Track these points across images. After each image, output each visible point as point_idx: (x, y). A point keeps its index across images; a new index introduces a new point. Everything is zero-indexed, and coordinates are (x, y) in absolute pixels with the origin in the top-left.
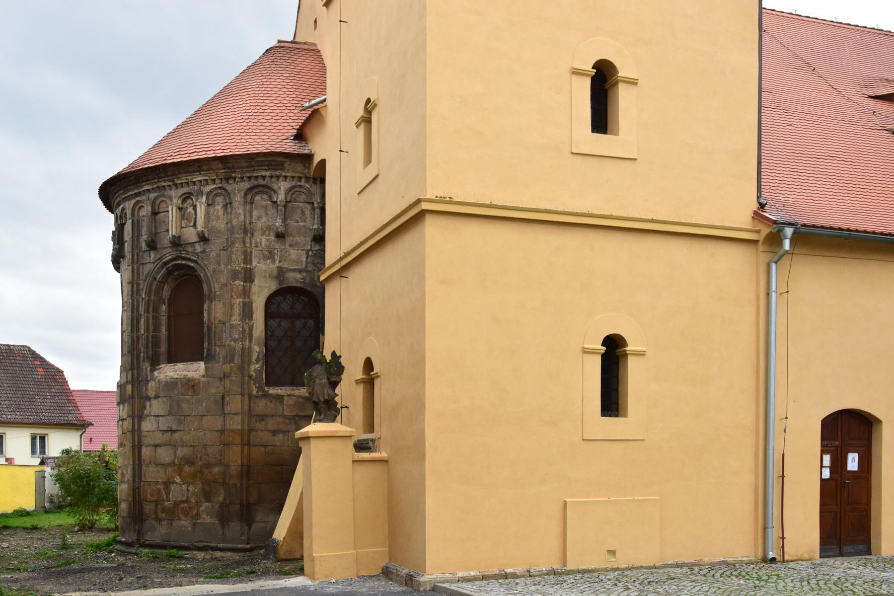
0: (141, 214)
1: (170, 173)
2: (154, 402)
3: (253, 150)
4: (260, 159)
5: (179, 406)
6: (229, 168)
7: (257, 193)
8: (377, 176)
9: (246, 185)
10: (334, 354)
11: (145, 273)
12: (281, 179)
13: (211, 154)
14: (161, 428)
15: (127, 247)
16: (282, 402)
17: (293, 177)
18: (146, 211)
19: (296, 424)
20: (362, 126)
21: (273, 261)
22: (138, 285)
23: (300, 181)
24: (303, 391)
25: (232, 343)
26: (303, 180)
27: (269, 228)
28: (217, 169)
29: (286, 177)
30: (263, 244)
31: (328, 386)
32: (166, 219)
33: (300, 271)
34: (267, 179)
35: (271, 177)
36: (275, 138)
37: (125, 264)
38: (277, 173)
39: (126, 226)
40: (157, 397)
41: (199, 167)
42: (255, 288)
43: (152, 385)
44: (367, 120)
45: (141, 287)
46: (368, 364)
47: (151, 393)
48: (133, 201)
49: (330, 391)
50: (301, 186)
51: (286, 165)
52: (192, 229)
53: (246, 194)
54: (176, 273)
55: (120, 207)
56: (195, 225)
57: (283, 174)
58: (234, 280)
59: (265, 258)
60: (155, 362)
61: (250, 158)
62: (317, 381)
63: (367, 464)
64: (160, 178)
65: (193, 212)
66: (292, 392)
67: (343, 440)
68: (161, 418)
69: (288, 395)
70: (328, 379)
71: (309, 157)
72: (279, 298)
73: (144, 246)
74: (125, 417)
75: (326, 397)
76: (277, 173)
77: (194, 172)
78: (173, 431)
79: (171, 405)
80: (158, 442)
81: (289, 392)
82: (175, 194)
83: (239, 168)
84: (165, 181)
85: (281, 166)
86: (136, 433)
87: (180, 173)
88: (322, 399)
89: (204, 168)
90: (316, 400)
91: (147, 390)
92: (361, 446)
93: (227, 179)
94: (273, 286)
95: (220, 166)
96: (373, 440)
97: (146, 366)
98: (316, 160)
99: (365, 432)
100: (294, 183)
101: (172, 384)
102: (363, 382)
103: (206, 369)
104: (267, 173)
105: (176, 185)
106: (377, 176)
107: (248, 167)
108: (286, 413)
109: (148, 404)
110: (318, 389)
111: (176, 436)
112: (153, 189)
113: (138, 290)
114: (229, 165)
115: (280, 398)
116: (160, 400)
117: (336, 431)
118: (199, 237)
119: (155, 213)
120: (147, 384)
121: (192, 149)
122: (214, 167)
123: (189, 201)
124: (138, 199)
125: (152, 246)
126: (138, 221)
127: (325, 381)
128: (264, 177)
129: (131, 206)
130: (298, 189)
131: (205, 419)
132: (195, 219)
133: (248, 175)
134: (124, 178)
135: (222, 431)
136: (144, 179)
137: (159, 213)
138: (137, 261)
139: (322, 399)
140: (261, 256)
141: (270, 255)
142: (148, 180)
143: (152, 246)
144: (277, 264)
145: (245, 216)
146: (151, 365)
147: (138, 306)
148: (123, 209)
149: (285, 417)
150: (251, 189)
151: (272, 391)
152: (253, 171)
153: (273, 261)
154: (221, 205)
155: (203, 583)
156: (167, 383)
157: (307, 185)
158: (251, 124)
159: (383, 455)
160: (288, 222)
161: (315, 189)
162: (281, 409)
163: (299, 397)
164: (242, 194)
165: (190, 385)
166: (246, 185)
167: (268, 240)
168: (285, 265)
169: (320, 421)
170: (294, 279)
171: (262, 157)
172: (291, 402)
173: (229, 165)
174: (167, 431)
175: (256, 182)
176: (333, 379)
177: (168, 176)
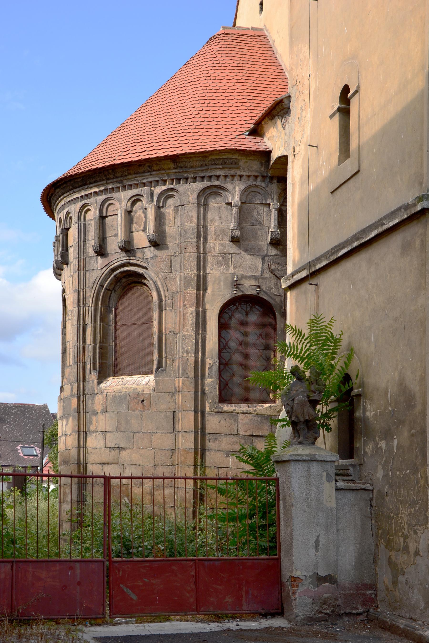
0: (87, 218)
1: (119, 175)
2: (101, 417)
3: (206, 148)
4: (214, 157)
5: (127, 421)
6: (181, 167)
7: (211, 194)
8: (358, 172)
9: (199, 186)
11: (92, 280)
12: (236, 178)
13: (162, 154)
14: (108, 445)
15: (72, 254)
17: (249, 176)
18: (92, 215)
20: (337, 118)
21: (228, 267)
22: (85, 293)
23: (256, 180)
25: (185, 355)
26: (259, 179)
27: (223, 232)
28: (169, 169)
29: (241, 176)
30: (217, 248)
32: (115, 224)
33: (256, 278)
34: (222, 178)
35: (226, 176)
36: (228, 133)
37: (69, 271)
38: (232, 172)
39: (70, 231)
40: (104, 411)
41: (149, 167)
42: (208, 296)
43: (99, 399)
44: (344, 111)
45: (88, 295)
47: (98, 407)
48: (80, 204)
49: (311, 411)
50: (256, 186)
51: (241, 163)
52: (142, 233)
53: (199, 196)
54: (124, 280)
55: (65, 211)
56: (145, 230)
57: (239, 173)
58: (186, 287)
59: (219, 264)
60: (102, 376)
61: (204, 155)
64: (109, 179)
65: (143, 215)
68: (108, 435)
69: (243, 413)
71: (268, 154)
72: (233, 308)
73: (91, 252)
74: (69, 432)
76: (232, 172)
77: (144, 172)
78: (120, 449)
79: (118, 420)
80: (105, 460)
82: (123, 197)
83: (192, 167)
84: (113, 183)
85: (235, 164)
86: (82, 449)
87: (129, 174)
88: (302, 419)
89: (155, 168)
90: (296, 420)
91: (93, 404)
93: (179, 180)
94: (227, 295)
95: (172, 165)
97: (93, 377)
98: (274, 156)
99: (342, 458)
100: (249, 183)
101: (122, 398)
103: (157, 382)
104: (221, 173)
105: (125, 186)
106: (358, 172)
107: (202, 166)
109: (94, 418)
111: (124, 454)
112: (100, 191)
113: (85, 298)
114: (181, 164)
115: (235, 414)
116: (107, 415)
118: (150, 242)
119: (102, 218)
120: (94, 397)
121: (174, 144)
122: (165, 167)
123: (139, 204)
124: (84, 202)
125: (101, 252)
126: (85, 225)
128: (218, 177)
129: (78, 210)
130: (253, 189)
131: (155, 436)
132: (145, 223)
133: (202, 175)
134: (70, 181)
135: (173, 451)
136: (92, 180)
137: (107, 216)
138: (83, 267)
139: (302, 419)
140: (215, 262)
141: (225, 259)
142: (96, 182)
143: (101, 252)
144: (231, 271)
145: (198, 219)
146: (99, 377)
147: (84, 315)
148: (68, 213)
150: (204, 189)
151: (227, 407)
152: (207, 170)
153: (228, 267)
154: (173, 207)
155: (201, 621)
156: (114, 397)
157: (263, 185)
158: (202, 119)
160: (244, 225)
161: (274, 187)
164: (195, 195)
165: (140, 400)
166: (199, 186)
167: (222, 245)
168: (240, 271)
170: (250, 288)
171: (216, 155)
173: (181, 164)
174: (114, 448)
175: (209, 183)
177: (117, 177)
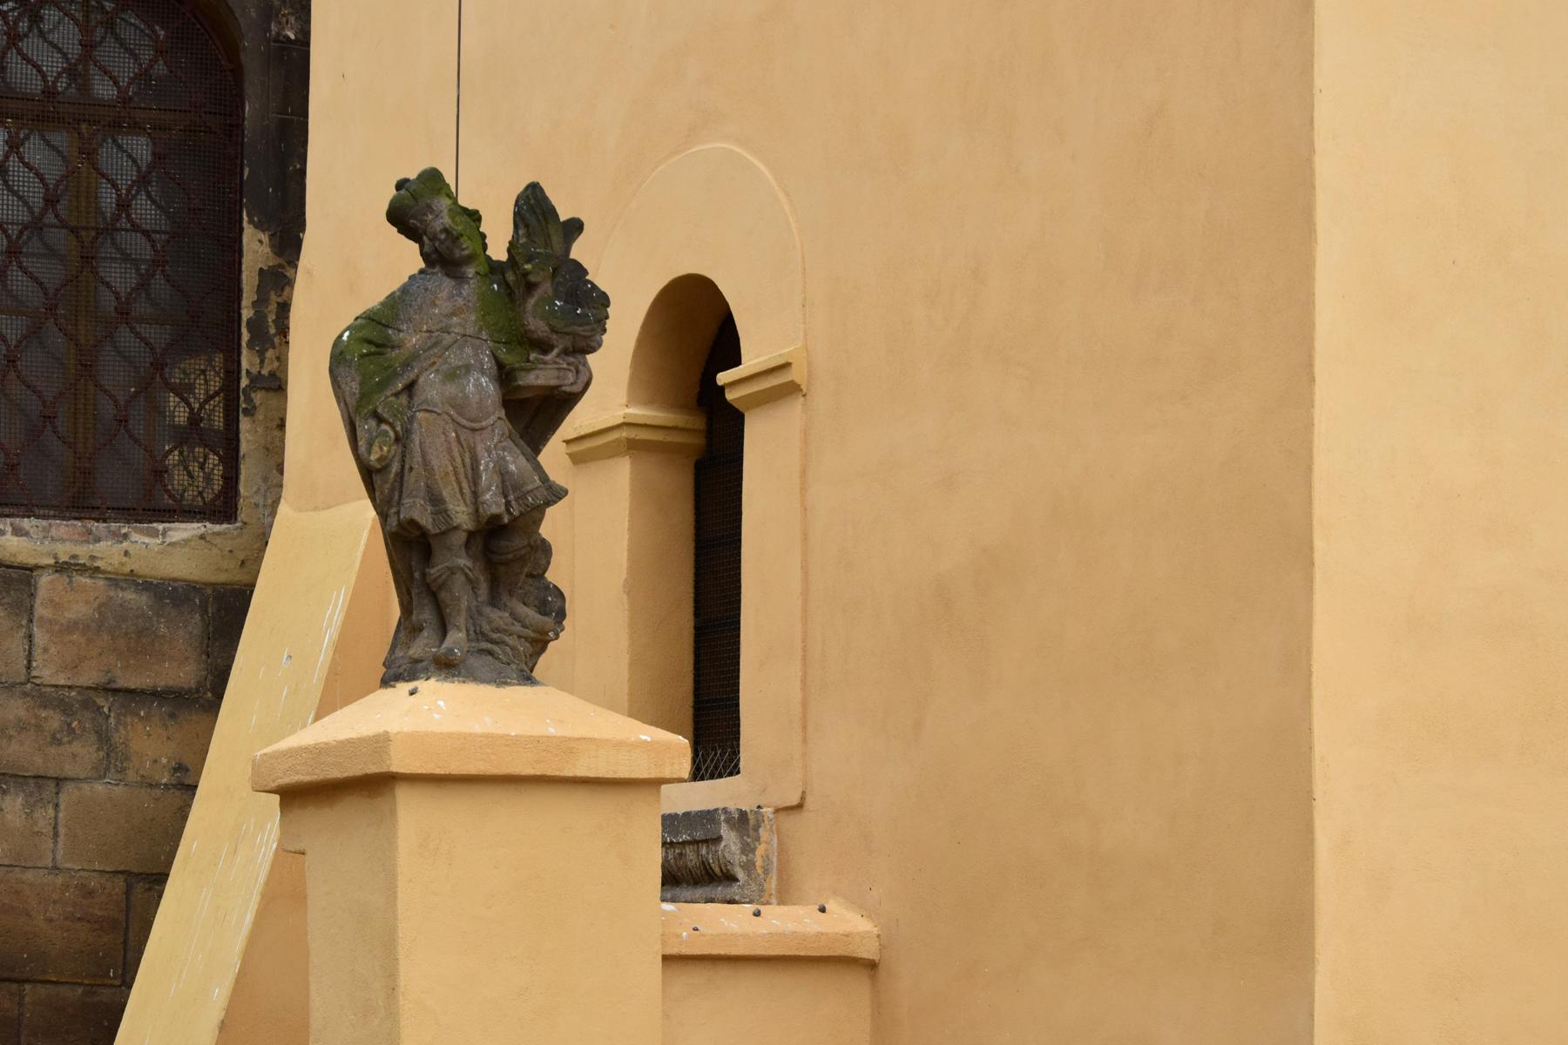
10: (533, 208)
16: (24, 609)
19: (104, 738)
24: (556, 351)
31: (496, 416)
46: (698, 328)
49: (516, 463)
62: (432, 387)
63: (750, 984)
66: (83, 551)
67: (607, 803)
69: (61, 568)
70: (504, 375)
75: (493, 502)
81: (64, 551)
88: (461, 514)
90: (425, 519)
92: (694, 866)
96: (743, 821)
102: (633, 447)
108: (47, 673)
110: (435, 444)
117: (567, 746)
127: (481, 387)
149: (43, 696)
159: (846, 924)
162: (17, 646)
163: (118, 580)
169: (447, 667)
172: (79, 609)
176: (541, 376)
